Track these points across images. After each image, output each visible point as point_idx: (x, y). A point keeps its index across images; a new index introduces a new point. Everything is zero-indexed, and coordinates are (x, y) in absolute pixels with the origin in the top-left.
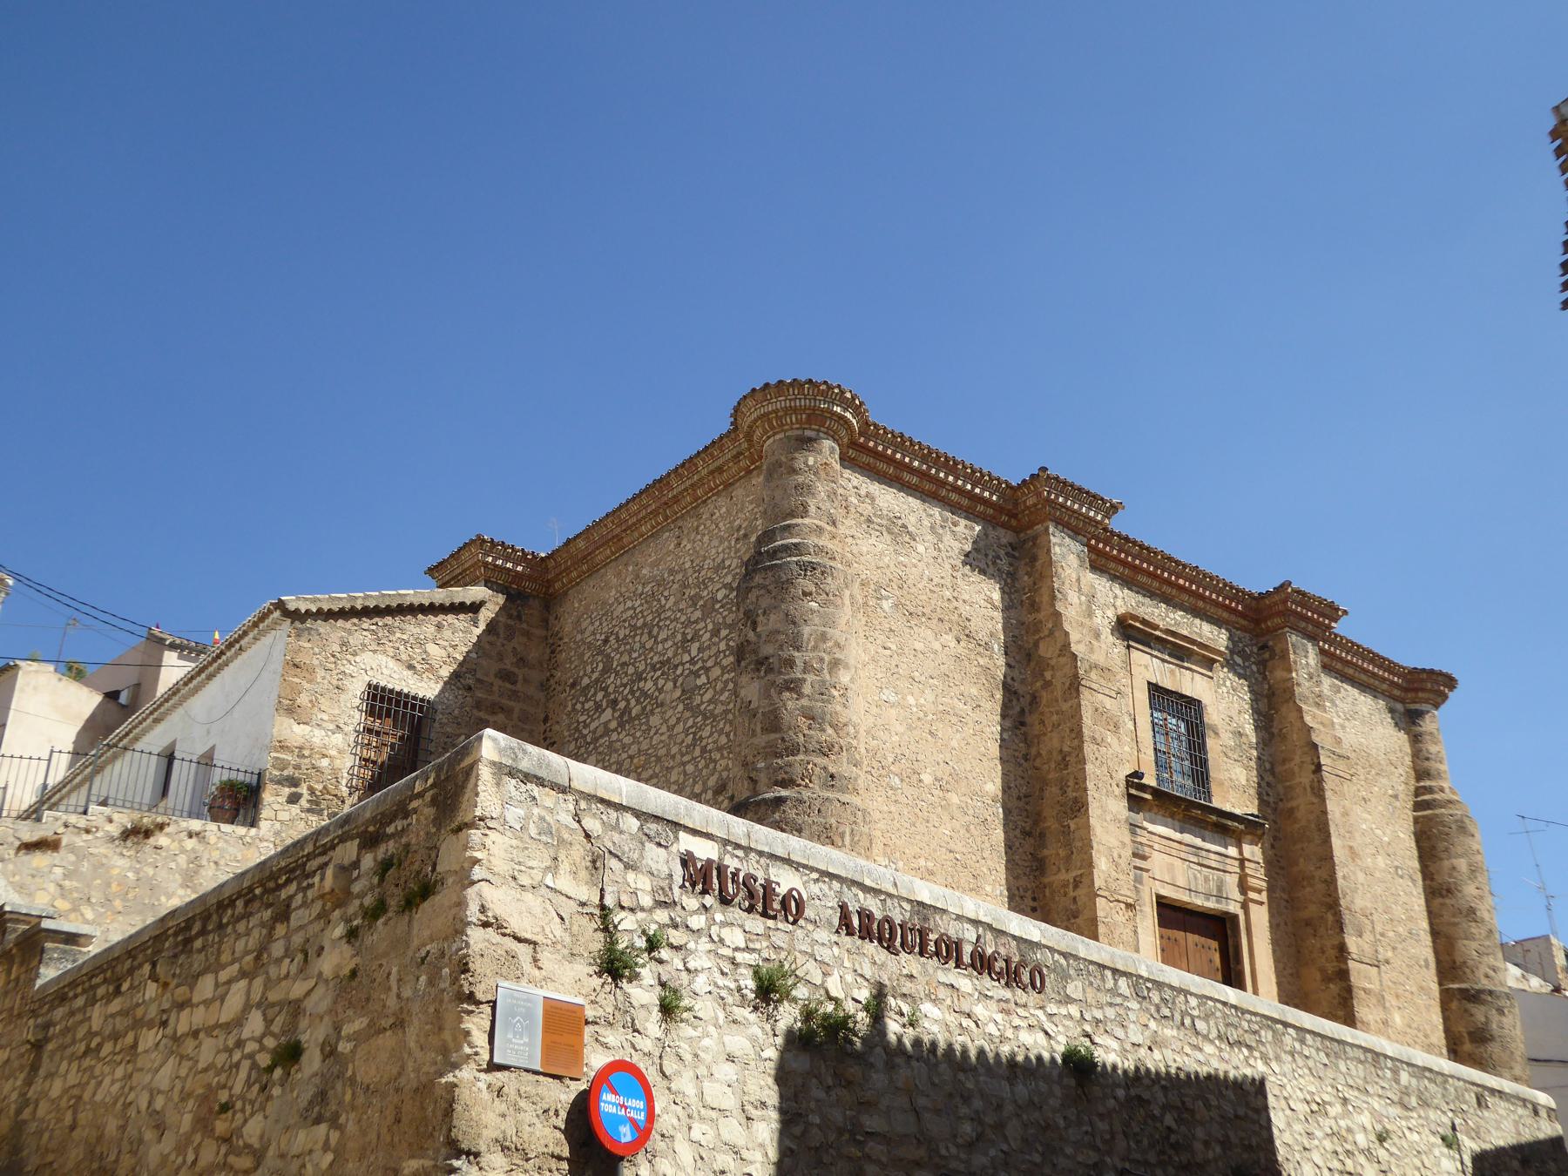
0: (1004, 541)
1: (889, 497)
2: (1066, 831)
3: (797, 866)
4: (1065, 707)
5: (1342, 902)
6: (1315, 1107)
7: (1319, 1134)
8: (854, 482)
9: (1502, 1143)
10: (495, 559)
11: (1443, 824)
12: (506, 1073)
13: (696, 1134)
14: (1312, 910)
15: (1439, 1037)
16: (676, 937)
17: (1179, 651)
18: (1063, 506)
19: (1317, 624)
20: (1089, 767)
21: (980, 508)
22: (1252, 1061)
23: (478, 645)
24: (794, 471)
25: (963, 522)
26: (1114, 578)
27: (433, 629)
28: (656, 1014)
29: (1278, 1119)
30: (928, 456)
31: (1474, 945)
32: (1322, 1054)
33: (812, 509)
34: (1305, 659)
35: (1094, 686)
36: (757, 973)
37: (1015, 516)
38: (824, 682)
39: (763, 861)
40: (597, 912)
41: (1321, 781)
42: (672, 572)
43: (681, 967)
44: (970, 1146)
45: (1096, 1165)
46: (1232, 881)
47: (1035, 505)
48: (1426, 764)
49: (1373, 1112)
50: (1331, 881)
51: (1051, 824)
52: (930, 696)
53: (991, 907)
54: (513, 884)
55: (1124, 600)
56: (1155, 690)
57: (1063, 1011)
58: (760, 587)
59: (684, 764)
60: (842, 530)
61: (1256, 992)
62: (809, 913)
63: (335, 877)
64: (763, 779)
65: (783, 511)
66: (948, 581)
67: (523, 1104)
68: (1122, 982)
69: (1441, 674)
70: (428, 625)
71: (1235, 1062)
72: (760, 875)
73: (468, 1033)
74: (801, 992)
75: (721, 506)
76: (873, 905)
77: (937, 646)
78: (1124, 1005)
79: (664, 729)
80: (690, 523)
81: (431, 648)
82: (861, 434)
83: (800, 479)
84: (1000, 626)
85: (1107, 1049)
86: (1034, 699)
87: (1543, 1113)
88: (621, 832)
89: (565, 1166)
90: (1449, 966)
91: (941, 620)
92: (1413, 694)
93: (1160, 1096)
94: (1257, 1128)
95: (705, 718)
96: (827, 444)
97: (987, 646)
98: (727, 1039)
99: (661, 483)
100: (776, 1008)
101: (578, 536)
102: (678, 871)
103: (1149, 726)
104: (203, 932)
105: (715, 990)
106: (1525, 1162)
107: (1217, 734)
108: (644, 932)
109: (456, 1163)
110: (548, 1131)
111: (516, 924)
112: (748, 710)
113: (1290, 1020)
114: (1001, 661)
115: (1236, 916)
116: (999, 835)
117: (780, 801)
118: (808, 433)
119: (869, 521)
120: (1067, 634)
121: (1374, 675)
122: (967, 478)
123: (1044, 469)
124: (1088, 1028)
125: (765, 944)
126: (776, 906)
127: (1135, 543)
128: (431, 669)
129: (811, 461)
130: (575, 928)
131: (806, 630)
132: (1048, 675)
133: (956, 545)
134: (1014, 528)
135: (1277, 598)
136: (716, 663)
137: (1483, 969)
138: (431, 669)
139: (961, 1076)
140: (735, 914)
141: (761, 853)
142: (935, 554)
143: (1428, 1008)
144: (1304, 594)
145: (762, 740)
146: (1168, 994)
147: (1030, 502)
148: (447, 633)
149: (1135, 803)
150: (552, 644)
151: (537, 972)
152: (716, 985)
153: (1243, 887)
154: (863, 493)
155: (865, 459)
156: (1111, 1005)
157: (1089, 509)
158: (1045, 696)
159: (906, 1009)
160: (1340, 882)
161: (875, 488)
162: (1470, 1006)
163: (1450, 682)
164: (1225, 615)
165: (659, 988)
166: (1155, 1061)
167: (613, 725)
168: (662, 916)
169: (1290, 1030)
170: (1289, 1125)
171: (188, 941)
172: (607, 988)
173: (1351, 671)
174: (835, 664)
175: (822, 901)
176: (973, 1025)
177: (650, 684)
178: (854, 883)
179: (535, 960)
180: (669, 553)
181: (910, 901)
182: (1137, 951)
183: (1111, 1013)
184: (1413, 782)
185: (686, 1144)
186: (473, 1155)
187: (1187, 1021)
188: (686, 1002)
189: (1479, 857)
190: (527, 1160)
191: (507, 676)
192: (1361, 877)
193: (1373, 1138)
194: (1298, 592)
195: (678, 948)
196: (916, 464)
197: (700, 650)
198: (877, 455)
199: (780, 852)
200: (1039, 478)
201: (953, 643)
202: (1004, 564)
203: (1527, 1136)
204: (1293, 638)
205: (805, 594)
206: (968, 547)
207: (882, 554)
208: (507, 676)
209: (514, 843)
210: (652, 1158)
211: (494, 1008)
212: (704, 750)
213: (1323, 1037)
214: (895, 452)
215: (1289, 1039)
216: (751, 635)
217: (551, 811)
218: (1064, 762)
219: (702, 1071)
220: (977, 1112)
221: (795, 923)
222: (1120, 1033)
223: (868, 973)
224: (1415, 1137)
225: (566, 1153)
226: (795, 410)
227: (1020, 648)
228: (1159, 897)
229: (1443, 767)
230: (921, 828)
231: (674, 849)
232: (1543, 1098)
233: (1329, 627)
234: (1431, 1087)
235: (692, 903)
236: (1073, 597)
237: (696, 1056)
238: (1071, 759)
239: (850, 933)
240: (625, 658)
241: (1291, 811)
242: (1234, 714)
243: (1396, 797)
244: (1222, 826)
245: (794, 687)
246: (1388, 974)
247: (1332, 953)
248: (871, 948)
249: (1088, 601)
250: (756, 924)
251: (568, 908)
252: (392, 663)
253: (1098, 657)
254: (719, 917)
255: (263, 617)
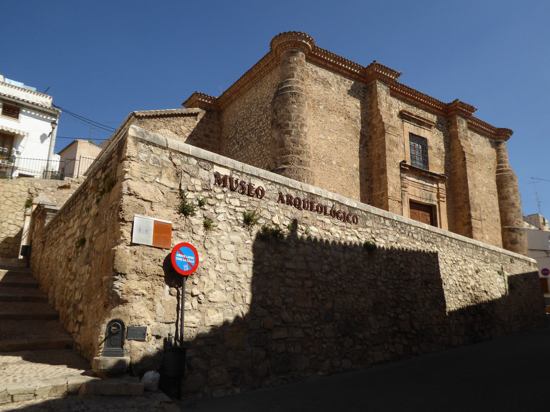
0: (362, 87)
1: (322, 72)
2: (380, 179)
3: (262, 179)
4: (380, 139)
5: (470, 201)
6: (454, 262)
7: (455, 270)
8: (310, 67)
9: (518, 273)
10: (202, 99)
11: (505, 177)
12: (138, 247)
13: (218, 268)
14: (461, 204)
15: (500, 242)
16: (211, 201)
17: (420, 122)
18: (381, 74)
19: (467, 113)
20: (387, 159)
21: (354, 76)
22: (433, 248)
23: (197, 126)
24: (290, 63)
25: (348, 80)
26: (399, 99)
27: (183, 121)
28: (202, 228)
29: (441, 266)
30: (336, 58)
31: (513, 214)
32: (458, 246)
33: (296, 75)
34: (462, 125)
35: (390, 133)
36: (244, 214)
37: (365, 78)
38: (298, 131)
39: (248, 177)
40: (179, 192)
41: (465, 163)
42: (254, 100)
43: (213, 211)
44: (327, 273)
45: (374, 279)
46: (434, 195)
47: (372, 74)
48: (501, 159)
49: (475, 264)
50: (467, 194)
51: (375, 177)
52: (335, 137)
53: (339, 195)
54: (142, 180)
55: (402, 106)
56: (412, 135)
57: (365, 230)
58: (278, 101)
59: (258, 160)
60: (306, 83)
61: (441, 227)
62: (266, 195)
63: (93, 182)
64: (279, 162)
65: (286, 77)
66: (342, 100)
67: (145, 257)
68: (387, 222)
69: (508, 130)
70: (181, 120)
71: (427, 247)
72: (247, 182)
73: (122, 232)
74: (261, 221)
75: (269, 78)
76: (293, 194)
77: (338, 120)
78: (393, 230)
79: (252, 150)
80: (260, 84)
81: (182, 127)
82: (312, 50)
83: (292, 65)
84: (360, 114)
85: (380, 243)
86: (371, 138)
87: (532, 265)
88: (189, 164)
89: (163, 278)
90: (505, 221)
91: (340, 112)
92: (498, 136)
93: (399, 258)
94: (433, 268)
95: (264, 145)
96: (301, 53)
97: (355, 121)
98: (231, 237)
99: (250, 71)
100: (252, 226)
101: (226, 91)
102: (213, 179)
103: (409, 147)
104: (72, 205)
105: (227, 220)
106: (525, 279)
107: (432, 149)
108: (198, 199)
109: (116, 277)
110: (155, 267)
111: (142, 194)
112: (274, 141)
113: (447, 235)
114: (360, 126)
115: (435, 206)
116: (358, 180)
117: (284, 169)
118: (294, 50)
119: (316, 80)
120: (381, 116)
121: (485, 130)
122: (349, 65)
123: (375, 61)
124: (373, 236)
125: (248, 205)
126: (253, 192)
127: (406, 87)
128: (183, 134)
129: (295, 59)
130: (169, 197)
131: (293, 114)
132: (375, 130)
133: (345, 88)
134: (364, 82)
135: (454, 105)
136: (267, 128)
137: (516, 222)
138: (183, 134)
139: (325, 251)
140: (236, 194)
141: (248, 174)
142: (338, 91)
143: (497, 234)
144: (463, 103)
145: (278, 150)
146: (403, 226)
147: (370, 73)
148: (187, 123)
149: (403, 170)
150: (221, 126)
151: (152, 212)
152: (227, 218)
153: (438, 196)
154: (314, 70)
155: (314, 59)
156: (382, 228)
157: (390, 75)
158: (374, 136)
159: (304, 228)
160: (470, 195)
161: (317, 69)
162: (511, 233)
163: (511, 132)
164: (436, 111)
165: (204, 219)
166: (397, 246)
167: (238, 149)
168: (206, 194)
169: (447, 238)
170: (445, 267)
171: (70, 209)
172: (182, 218)
173: (478, 129)
174: (302, 125)
175: (272, 191)
176: (330, 234)
177: (248, 136)
178: (285, 185)
179: (152, 208)
180: (254, 94)
181: (307, 192)
182: (402, 214)
183: (382, 231)
184: (496, 164)
185: (213, 272)
186: (124, 275)
187: (410, 234)
188: (215, 224)
189: (517, 188)
190: (147, 276)
191: (207, 136)
192: (477, 193)
193: (474, 272)
194: (461, 102)
195: (212, 205)
196: (332, 60)
197: (262, 124)
198: (318, 58)
199: (255, 174)
200: (373, 65)
201: (344, 120)
202: (361, 94)
203: (526, 271)
204: (459, 118)
205: (292, 103)
206: (349, 89)
207: (320, 91)
208: (207, 136)
209: (143, 166)
210: (199, 275)
211: (133, 224)
212: (264, 155)
213: (459, 240)
214: (324, 57)
215: (447, 241)
216: (275, 117)
217: (159, 155)
218: (379, 157)
219: (221, 247)
220: (330, 262)
221: (261, 198)
222: (385, 238)
223: (289, 215)
224: (489, 271)
225: (163, 274)
226: (290, 42)
227: (366, 121)
228: (410, 200)
229: (507, 160)
230: (332, 178)
231: (212, 171)
232: (533, 260)
233: (471, 114)
234: (495, 256)
235: (218, 190)
236: (384, 104)
237: (219, 242)
238: (382, 156)
239: (283, 202)
240: (241, 128)
241: (455, 173)
242: (438, 142)
243: (490, 169)
244: (433, 178)
245: (289, 133)
246: (484, 224)
247: (466, 216)
248: (291, 208)
249: (389, 106)
250: (245, 198)
251: (166, 190)
252: (170, 132)
253: (392, 123)
254: (229, 195)
255: (130, 118)
